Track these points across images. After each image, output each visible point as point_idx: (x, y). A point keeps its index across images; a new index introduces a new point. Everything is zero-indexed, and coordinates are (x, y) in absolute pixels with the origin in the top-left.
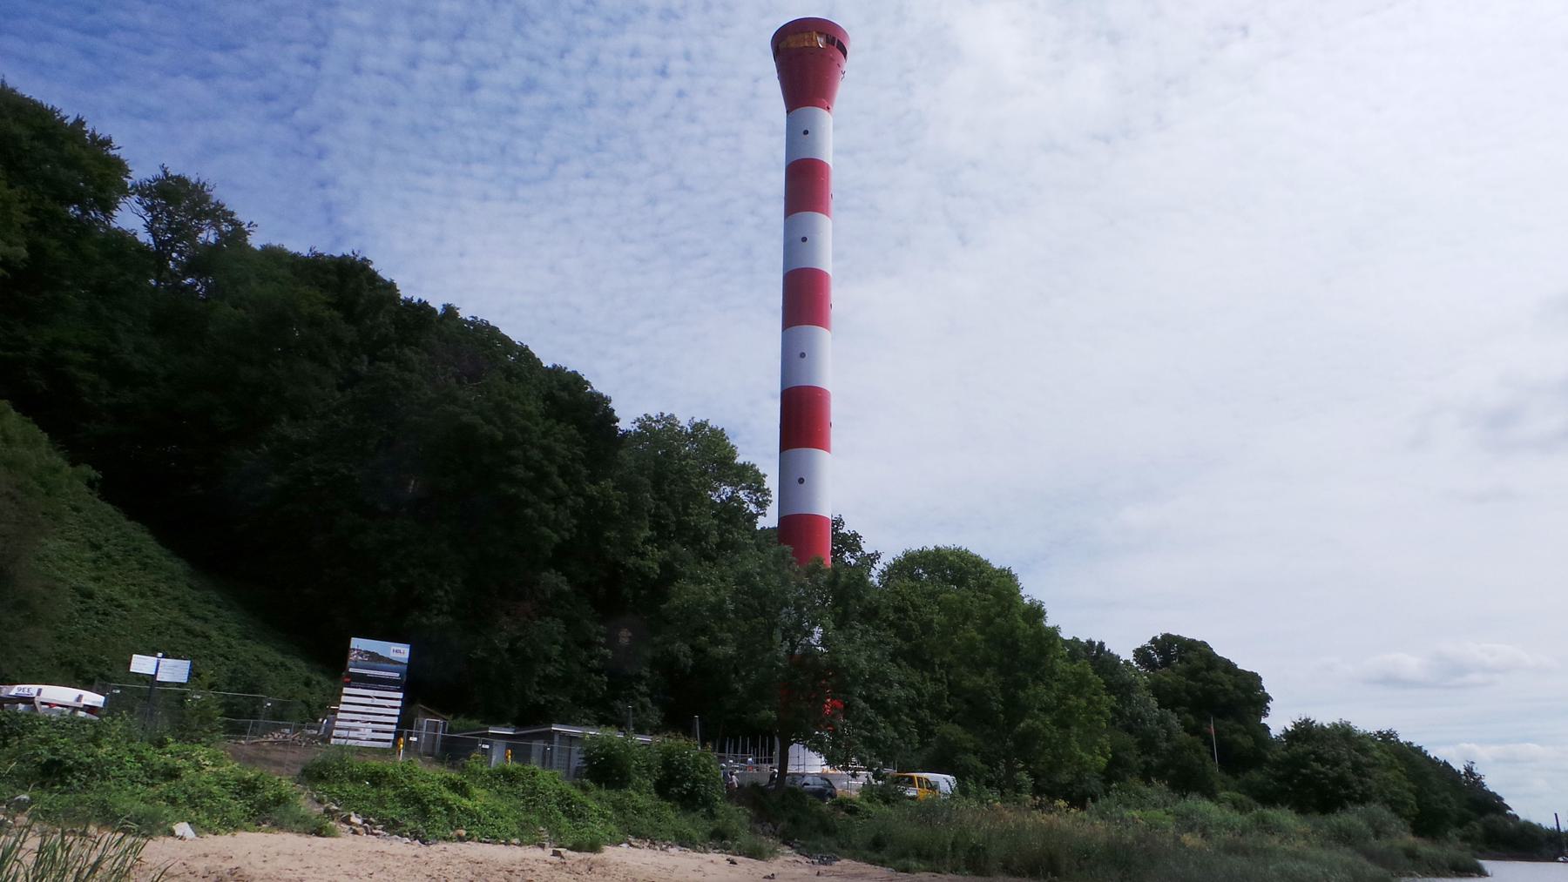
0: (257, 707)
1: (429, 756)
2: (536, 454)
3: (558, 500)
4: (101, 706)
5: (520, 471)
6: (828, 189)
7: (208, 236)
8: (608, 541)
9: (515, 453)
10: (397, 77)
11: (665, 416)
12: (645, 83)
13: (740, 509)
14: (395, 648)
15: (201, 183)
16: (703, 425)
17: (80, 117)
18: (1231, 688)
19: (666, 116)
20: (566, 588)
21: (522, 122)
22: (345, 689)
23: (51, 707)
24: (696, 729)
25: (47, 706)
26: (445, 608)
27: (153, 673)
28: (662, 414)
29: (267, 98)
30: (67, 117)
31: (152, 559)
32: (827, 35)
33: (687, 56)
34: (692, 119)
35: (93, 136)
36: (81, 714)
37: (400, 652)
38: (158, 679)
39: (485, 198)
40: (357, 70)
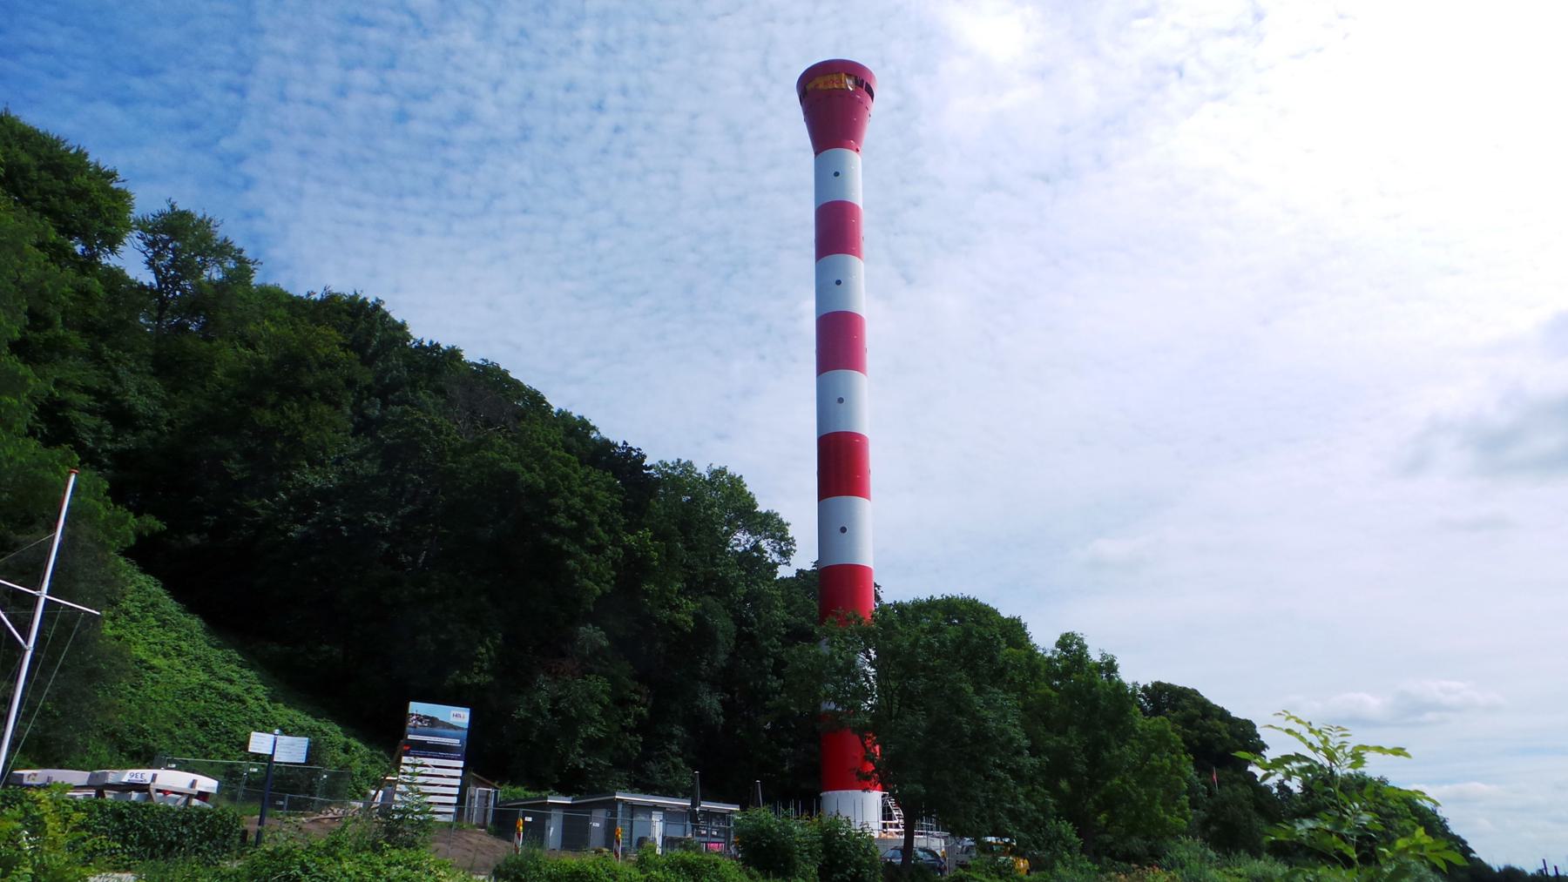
0: (314, 779)
1: (482, 828)
2: (577, 502)
3: (598, 549)
4: (214, 791)
5: (561, 520)
6: (858, 233)
7: (214, 274)
8: (646, 594)
9: (556, 501)
10: (326, 107)
11: (682, 462)
13: (760, 559)
15: (207, 218)
16: (722, 471)
17: (81, 148)
18: (1228, 736)
19: (604, 151)
20: (605, 643)
21: (455, 154)
22: (404, 758)
24: (758, 793)
25: (161, 794)
26: (486, 666)
27: (270, 753)
28: (679, 461)
29: (189, 126)
31: (170, 615)
32: (856, 78)
33: (624, 91)
34: (630, 155)
35: (97, 167)
36: (195, 802)
37: (460, 716)
39: (420, 232)
40: (283, 98)
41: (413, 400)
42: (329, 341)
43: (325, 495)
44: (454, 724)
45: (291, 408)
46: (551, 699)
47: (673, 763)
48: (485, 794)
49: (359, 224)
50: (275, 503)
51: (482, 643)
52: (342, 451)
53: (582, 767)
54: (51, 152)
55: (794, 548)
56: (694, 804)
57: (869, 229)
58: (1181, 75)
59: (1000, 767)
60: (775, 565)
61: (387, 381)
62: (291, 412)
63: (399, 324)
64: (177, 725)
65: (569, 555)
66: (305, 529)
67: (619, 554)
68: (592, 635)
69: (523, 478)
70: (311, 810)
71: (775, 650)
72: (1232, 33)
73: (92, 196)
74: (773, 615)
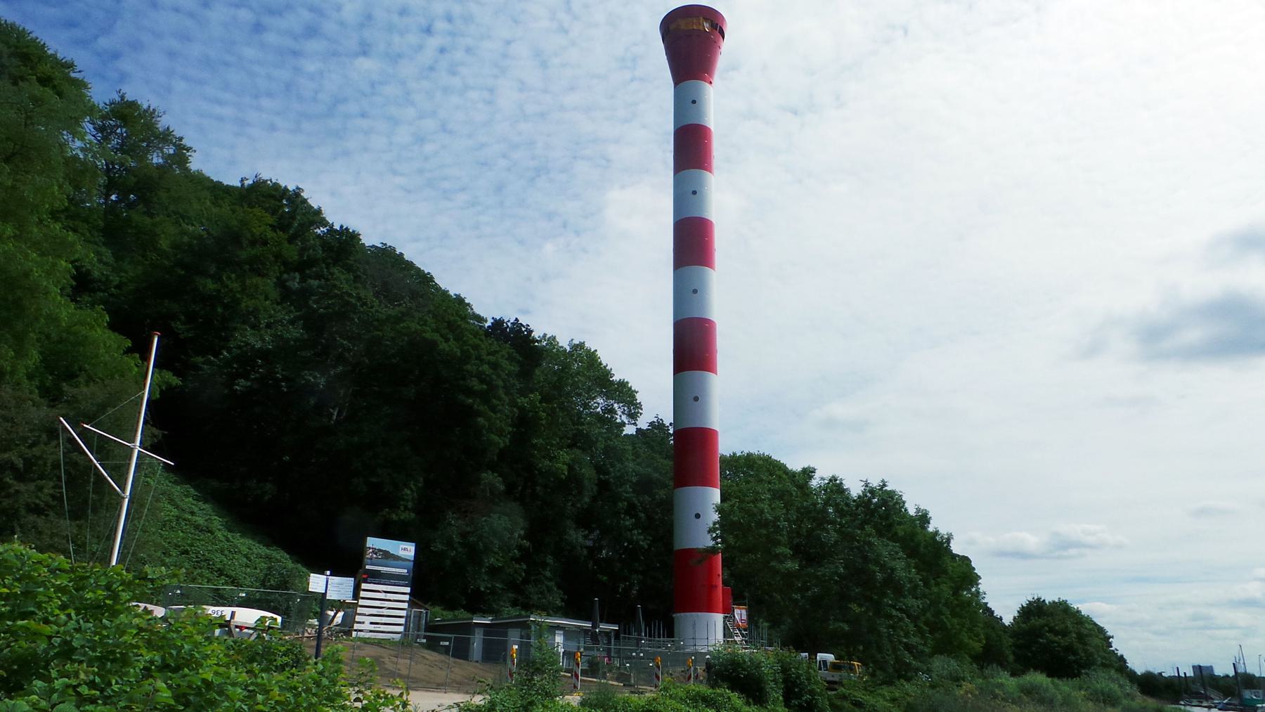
5: (475, 384)
8: (534, 446)
10: (191, 15)
12: (413, 39)
16: (581, 345)
19: (432, 69)
22: (363, 584)
26: (410, 505)
27: (324, 592)
28: (545, 335)
32: (712, 21)
33: (449, 19)
34: (453, 72)
37: (407, 550)
38: (328, 598)
39: (273, 128)
42: (260, 222)
43: (264, 354)
44: (403, 557)
45: (229, 278)
47: (547, 587)
49: (220, 119)
51: (406, 486)
52: (271, 317)
53: (482, 589)
54: (18, 42)
55: (640, 411)
56: (594, 626)
58: (906, 32)
59: (893, 607)
60: (623, 424)
61: (305, 258)
64: (164, 553)
65: (479, 414)
66: (249, 384)
69: (441, 347)
70: (288, 629)
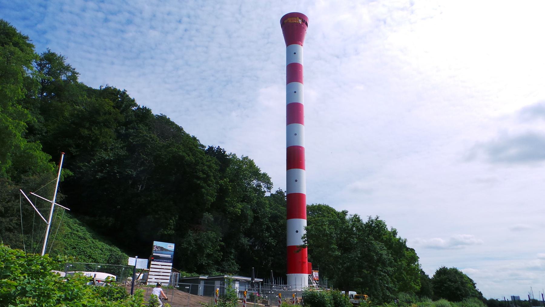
5: (201, 175)
7: (63, 77)
8: (226, 201)
10: (77, 15)
11: (232, 154)
13: (260, 191)
14: (169, 245)
15: (62, 56)
16: (247, 158)
19: (181, 38)
22: (152, 262)
23: (99, 282)
24: (272, 274)
26: (172, 227)
27: (135, 265)
30: (12, 26)
32: (302, 19)
33: (189, 17)
37: (171, 247)
38: (136, 268)
39: (113, 63)
40: (61, 10)
41: (137, 128)
42: (108, 104)
43: (109, 162)
45: (95, 129)
46: (194, 239)
48: (176, 275)
49: (90, 60)
50: (90, 164)
51: (171, 219)
55: (272, 186)
56: (252, 280)
57: (305, 73)
60: (265, 192)
61: (127, 120)
62: (95, 131)
63: (132, 100)
65: (203, 187)
67: (218, 187)
68: (209, 216)
69: (187, 159)
71: (267, 222)
72: (402, 9)
73: (20, 45)
74: (266, 210)
